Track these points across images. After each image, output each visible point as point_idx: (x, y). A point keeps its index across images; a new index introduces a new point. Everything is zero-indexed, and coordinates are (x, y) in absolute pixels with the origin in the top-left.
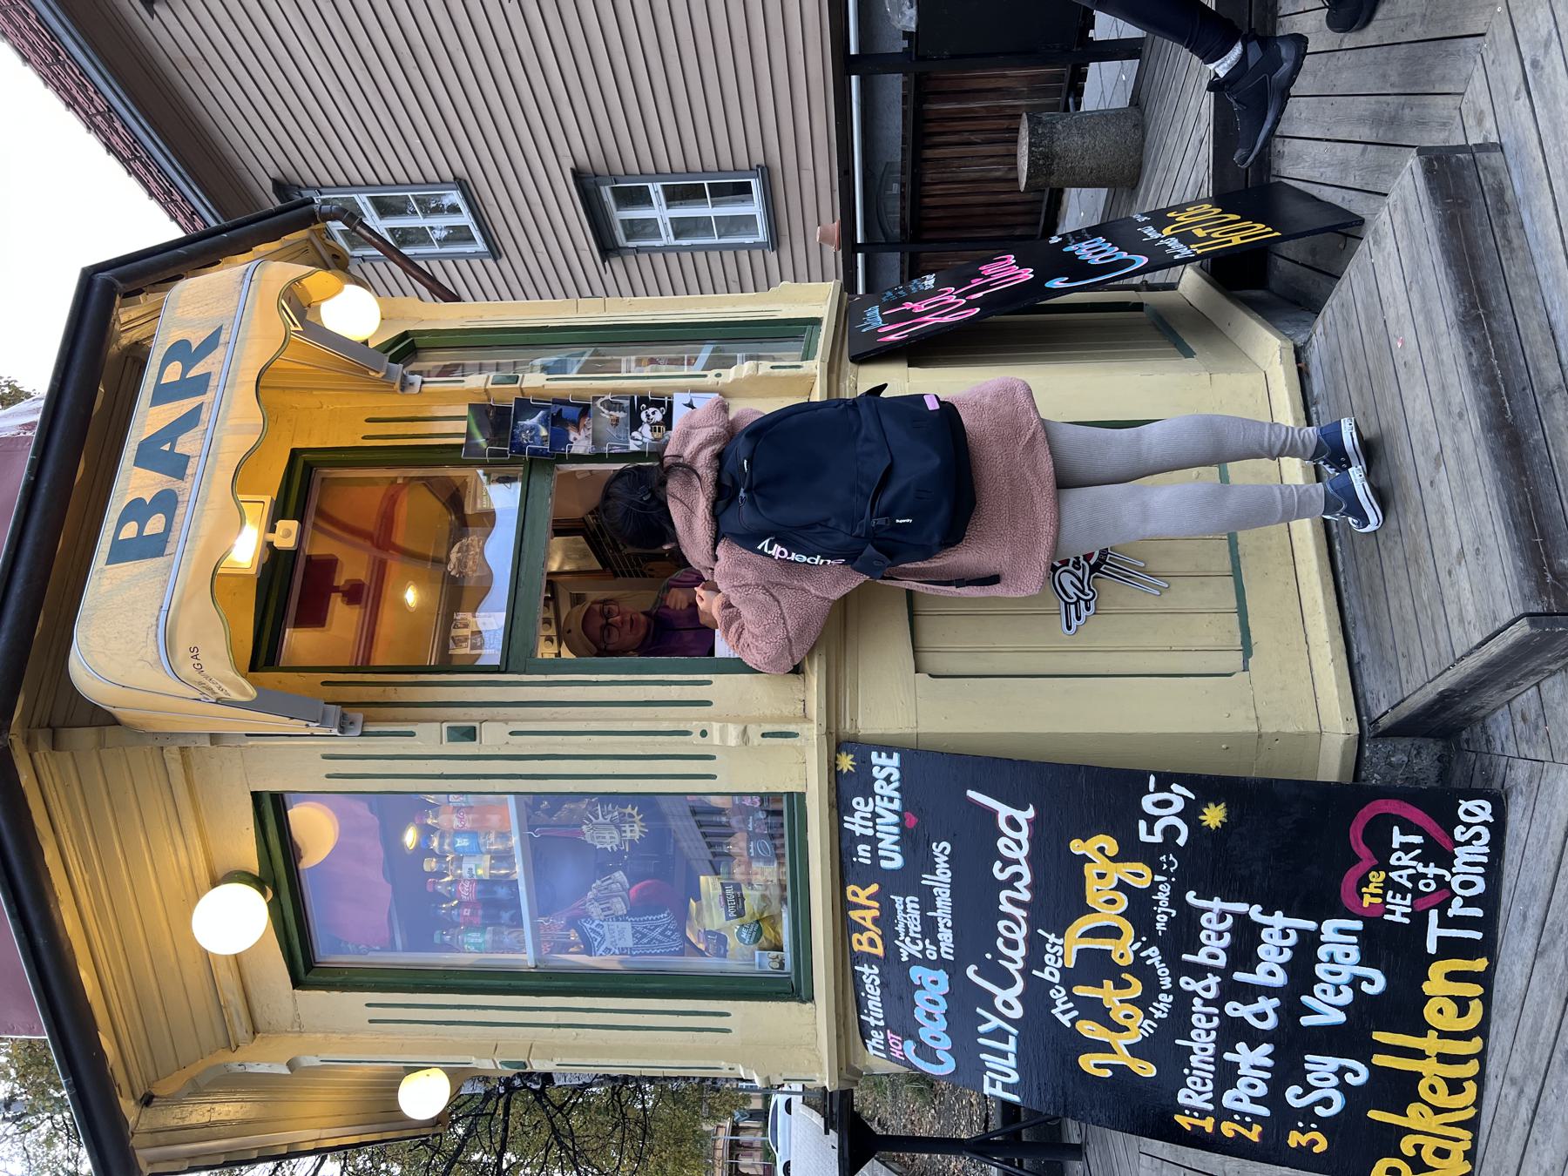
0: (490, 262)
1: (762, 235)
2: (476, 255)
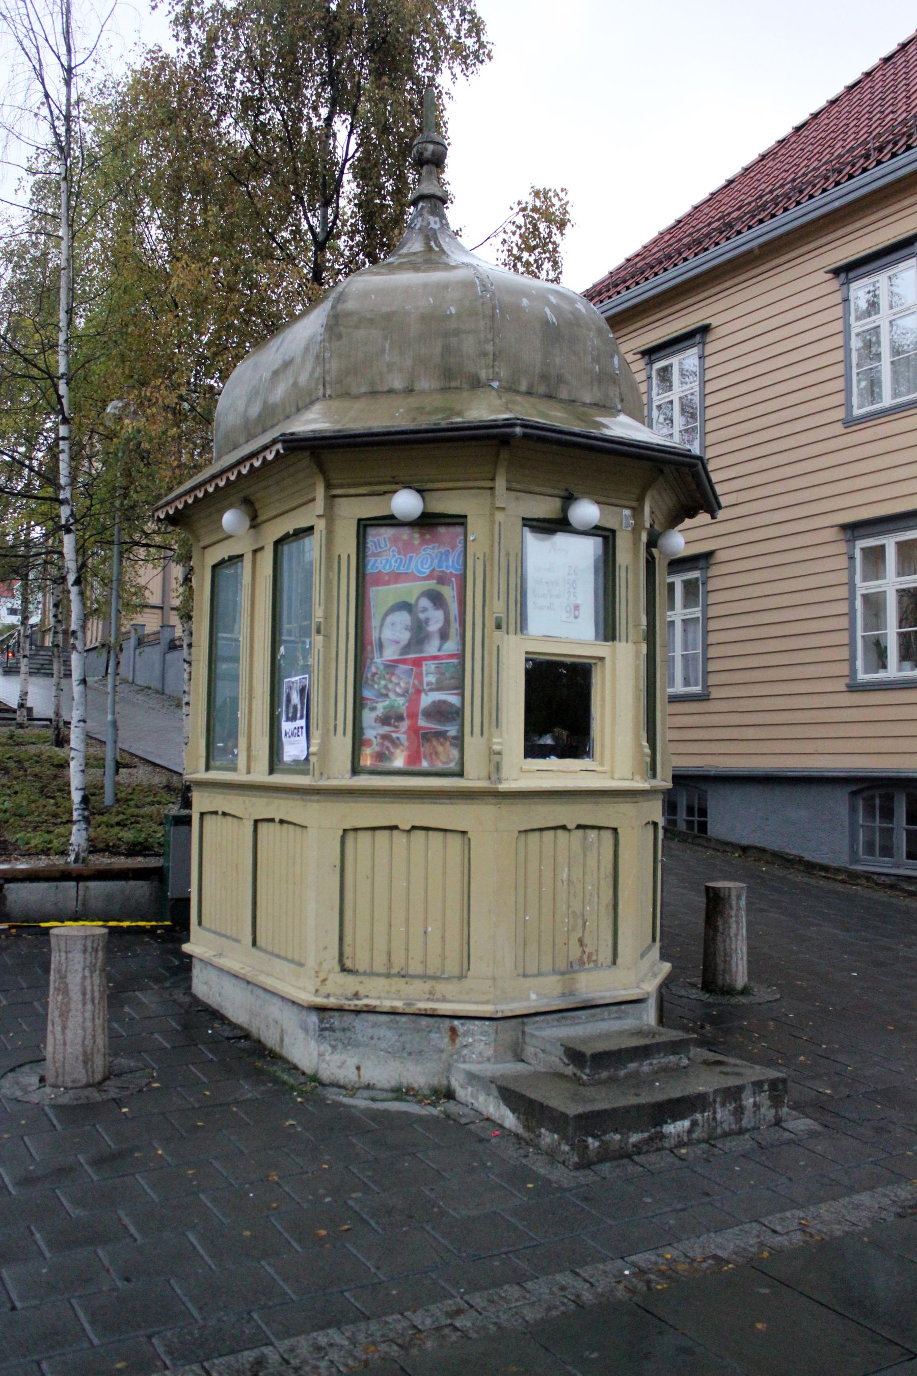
0: (840, 414)
1: (863, 676)
2: (848, 405)
